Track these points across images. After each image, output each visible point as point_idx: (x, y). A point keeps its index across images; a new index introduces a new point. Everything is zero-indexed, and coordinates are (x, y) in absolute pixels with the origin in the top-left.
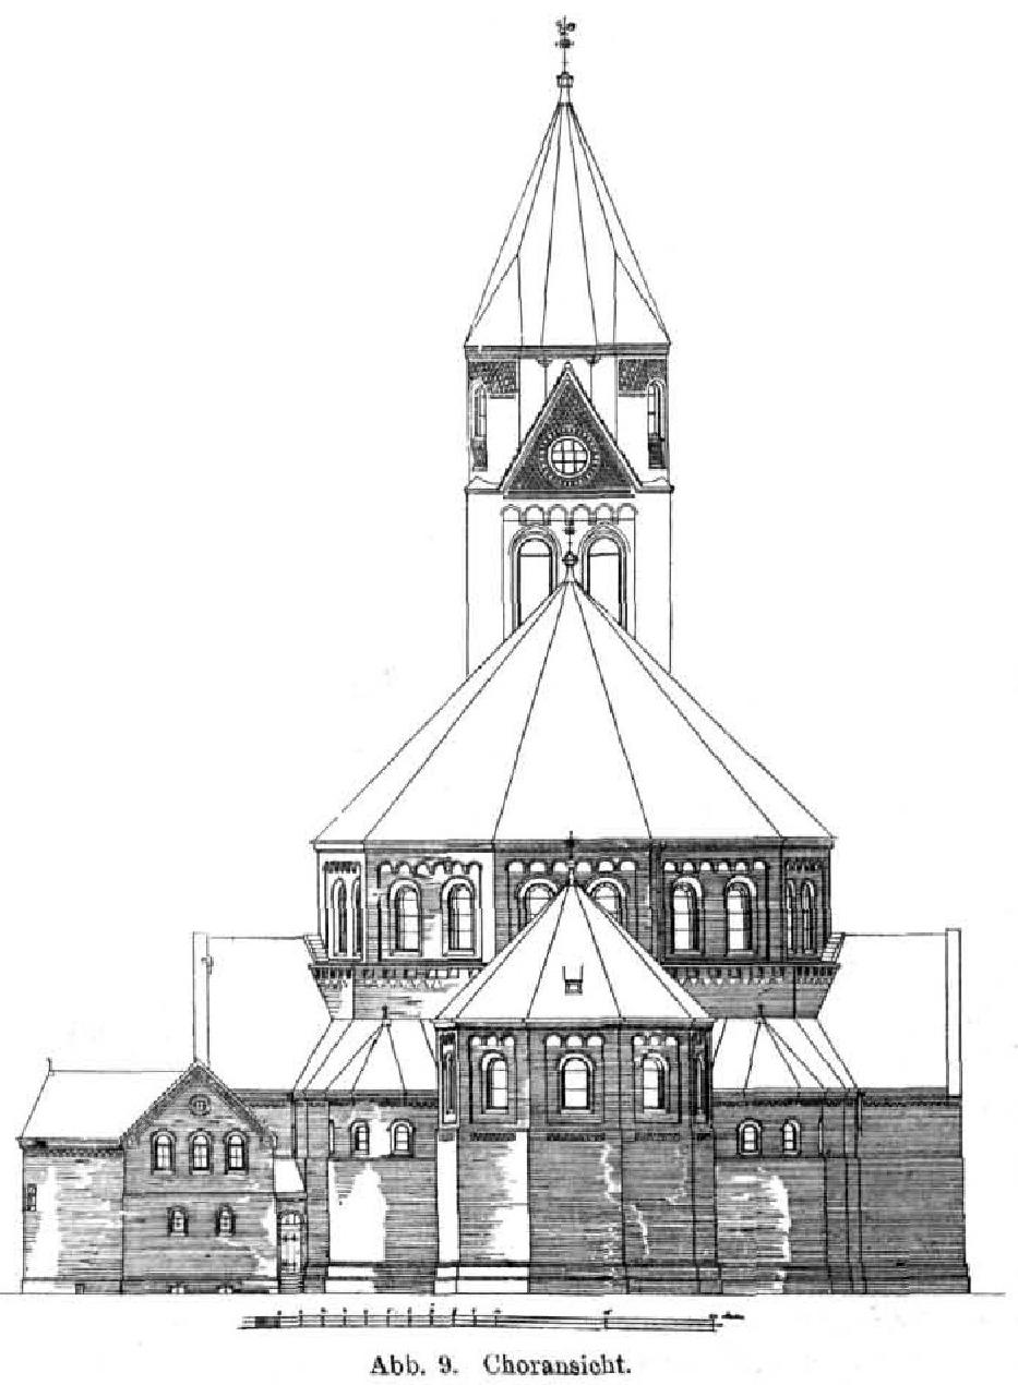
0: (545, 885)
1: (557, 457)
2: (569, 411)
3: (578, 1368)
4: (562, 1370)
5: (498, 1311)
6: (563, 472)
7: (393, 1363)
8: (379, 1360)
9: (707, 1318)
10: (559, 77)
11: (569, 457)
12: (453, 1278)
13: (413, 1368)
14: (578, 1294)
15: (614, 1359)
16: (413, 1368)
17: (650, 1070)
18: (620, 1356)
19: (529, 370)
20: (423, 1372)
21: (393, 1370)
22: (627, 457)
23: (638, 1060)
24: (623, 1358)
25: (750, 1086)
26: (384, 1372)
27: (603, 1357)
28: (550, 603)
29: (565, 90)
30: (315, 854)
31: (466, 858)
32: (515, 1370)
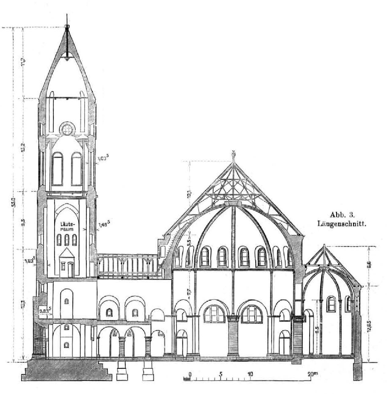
7: (337, 214)
8: (333, 213)
20: (345, 217)
21: (337, 216)
22: (285, 215)
24: (364, 222)
26: (334, 216)
30: (153, 367)
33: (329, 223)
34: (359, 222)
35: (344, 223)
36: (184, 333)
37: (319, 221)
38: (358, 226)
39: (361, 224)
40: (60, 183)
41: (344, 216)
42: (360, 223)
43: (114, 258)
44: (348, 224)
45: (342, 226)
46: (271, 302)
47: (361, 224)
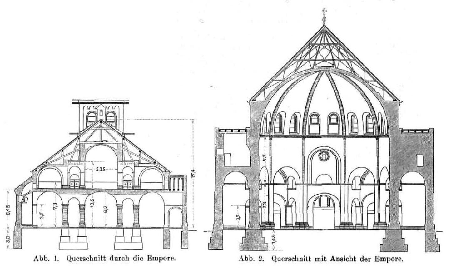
3: (342, 260)
7: (245, 258)
8: (36, 257)
15: (353, 257)
16: (250, 259)
18: (355, 257)
21: (245, 260)
23: (307, 58)
26: (37, 260)
28: (348, 68)
35: (290, 258)
36: (293, 202)
38: (304, 261)
39: (103, 259)
40: (142, 249)
41: (48, 259)
43: (114, 118)
44: (125, 259)
45: (341, 261)
46: (378, 169)
47: (103, 259)
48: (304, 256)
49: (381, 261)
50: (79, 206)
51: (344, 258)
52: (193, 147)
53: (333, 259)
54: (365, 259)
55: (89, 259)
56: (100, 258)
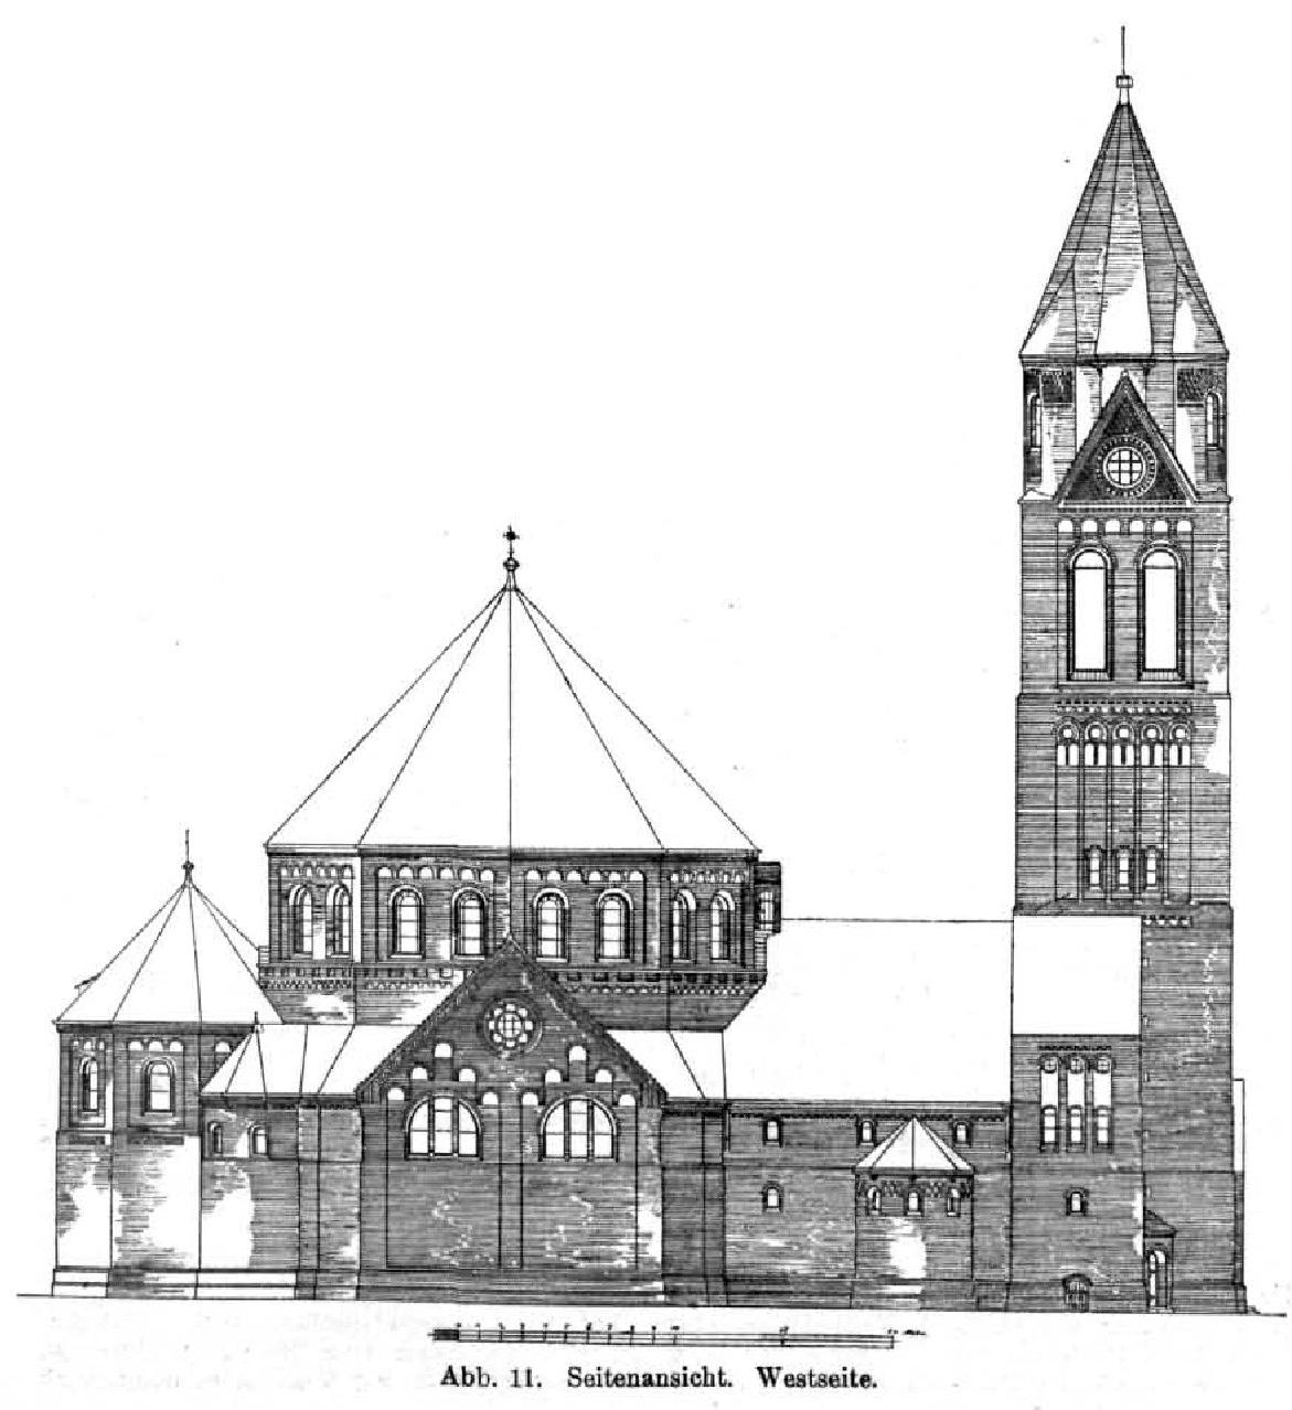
0: (618, 895)
1: (1136, 467)
2: (1122, 421)
3: (678, 1380)
4: (662, 1381)
5: (459, 1325)
6: (1119, 482)
7: (464, 1374)
8: (450, 1369)
9: (884, 1333)
10: (1119, 78)
11: (1125, 467)
12: (202, 1286)
13: (719, 1380)
14: (1043, 1311)
17: (161, 1074)
19: (1082, 379)
20: (495, 1385)
21: (464, 1382)
25: (323, 1091)
26: (455, 1382)
27: (479, 1368)
29: (1124, 91)
31: (340, 862)
32: (689, 1382)
33: (637, 1377)
34: (848, 1373)
37: (515, 1372)
42: (608, 1374)
45: (672, 1385)
48: (845, 1369)
49: (630, 1385)
50: (1018, 508)
51: (685, 1376)
52: (575, 695)
53: (452, 1376)
54: (616, 1380)
55: (702, 1378)
56: (849, 1378)
